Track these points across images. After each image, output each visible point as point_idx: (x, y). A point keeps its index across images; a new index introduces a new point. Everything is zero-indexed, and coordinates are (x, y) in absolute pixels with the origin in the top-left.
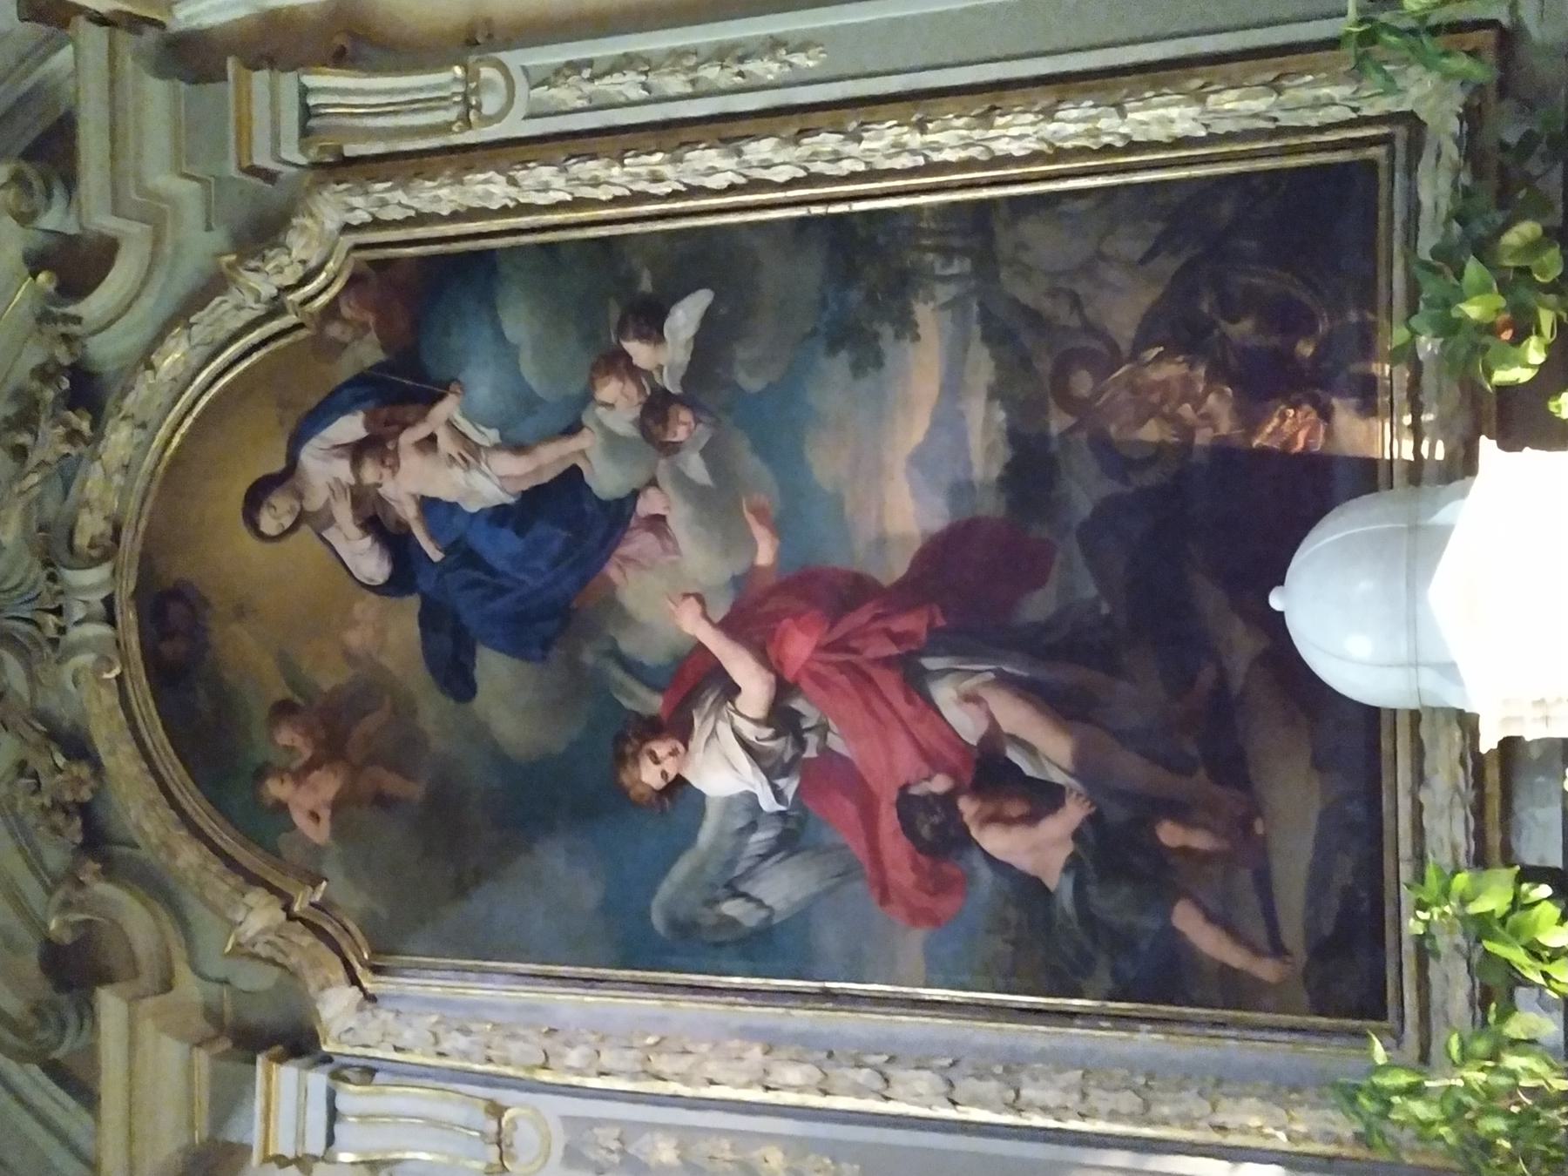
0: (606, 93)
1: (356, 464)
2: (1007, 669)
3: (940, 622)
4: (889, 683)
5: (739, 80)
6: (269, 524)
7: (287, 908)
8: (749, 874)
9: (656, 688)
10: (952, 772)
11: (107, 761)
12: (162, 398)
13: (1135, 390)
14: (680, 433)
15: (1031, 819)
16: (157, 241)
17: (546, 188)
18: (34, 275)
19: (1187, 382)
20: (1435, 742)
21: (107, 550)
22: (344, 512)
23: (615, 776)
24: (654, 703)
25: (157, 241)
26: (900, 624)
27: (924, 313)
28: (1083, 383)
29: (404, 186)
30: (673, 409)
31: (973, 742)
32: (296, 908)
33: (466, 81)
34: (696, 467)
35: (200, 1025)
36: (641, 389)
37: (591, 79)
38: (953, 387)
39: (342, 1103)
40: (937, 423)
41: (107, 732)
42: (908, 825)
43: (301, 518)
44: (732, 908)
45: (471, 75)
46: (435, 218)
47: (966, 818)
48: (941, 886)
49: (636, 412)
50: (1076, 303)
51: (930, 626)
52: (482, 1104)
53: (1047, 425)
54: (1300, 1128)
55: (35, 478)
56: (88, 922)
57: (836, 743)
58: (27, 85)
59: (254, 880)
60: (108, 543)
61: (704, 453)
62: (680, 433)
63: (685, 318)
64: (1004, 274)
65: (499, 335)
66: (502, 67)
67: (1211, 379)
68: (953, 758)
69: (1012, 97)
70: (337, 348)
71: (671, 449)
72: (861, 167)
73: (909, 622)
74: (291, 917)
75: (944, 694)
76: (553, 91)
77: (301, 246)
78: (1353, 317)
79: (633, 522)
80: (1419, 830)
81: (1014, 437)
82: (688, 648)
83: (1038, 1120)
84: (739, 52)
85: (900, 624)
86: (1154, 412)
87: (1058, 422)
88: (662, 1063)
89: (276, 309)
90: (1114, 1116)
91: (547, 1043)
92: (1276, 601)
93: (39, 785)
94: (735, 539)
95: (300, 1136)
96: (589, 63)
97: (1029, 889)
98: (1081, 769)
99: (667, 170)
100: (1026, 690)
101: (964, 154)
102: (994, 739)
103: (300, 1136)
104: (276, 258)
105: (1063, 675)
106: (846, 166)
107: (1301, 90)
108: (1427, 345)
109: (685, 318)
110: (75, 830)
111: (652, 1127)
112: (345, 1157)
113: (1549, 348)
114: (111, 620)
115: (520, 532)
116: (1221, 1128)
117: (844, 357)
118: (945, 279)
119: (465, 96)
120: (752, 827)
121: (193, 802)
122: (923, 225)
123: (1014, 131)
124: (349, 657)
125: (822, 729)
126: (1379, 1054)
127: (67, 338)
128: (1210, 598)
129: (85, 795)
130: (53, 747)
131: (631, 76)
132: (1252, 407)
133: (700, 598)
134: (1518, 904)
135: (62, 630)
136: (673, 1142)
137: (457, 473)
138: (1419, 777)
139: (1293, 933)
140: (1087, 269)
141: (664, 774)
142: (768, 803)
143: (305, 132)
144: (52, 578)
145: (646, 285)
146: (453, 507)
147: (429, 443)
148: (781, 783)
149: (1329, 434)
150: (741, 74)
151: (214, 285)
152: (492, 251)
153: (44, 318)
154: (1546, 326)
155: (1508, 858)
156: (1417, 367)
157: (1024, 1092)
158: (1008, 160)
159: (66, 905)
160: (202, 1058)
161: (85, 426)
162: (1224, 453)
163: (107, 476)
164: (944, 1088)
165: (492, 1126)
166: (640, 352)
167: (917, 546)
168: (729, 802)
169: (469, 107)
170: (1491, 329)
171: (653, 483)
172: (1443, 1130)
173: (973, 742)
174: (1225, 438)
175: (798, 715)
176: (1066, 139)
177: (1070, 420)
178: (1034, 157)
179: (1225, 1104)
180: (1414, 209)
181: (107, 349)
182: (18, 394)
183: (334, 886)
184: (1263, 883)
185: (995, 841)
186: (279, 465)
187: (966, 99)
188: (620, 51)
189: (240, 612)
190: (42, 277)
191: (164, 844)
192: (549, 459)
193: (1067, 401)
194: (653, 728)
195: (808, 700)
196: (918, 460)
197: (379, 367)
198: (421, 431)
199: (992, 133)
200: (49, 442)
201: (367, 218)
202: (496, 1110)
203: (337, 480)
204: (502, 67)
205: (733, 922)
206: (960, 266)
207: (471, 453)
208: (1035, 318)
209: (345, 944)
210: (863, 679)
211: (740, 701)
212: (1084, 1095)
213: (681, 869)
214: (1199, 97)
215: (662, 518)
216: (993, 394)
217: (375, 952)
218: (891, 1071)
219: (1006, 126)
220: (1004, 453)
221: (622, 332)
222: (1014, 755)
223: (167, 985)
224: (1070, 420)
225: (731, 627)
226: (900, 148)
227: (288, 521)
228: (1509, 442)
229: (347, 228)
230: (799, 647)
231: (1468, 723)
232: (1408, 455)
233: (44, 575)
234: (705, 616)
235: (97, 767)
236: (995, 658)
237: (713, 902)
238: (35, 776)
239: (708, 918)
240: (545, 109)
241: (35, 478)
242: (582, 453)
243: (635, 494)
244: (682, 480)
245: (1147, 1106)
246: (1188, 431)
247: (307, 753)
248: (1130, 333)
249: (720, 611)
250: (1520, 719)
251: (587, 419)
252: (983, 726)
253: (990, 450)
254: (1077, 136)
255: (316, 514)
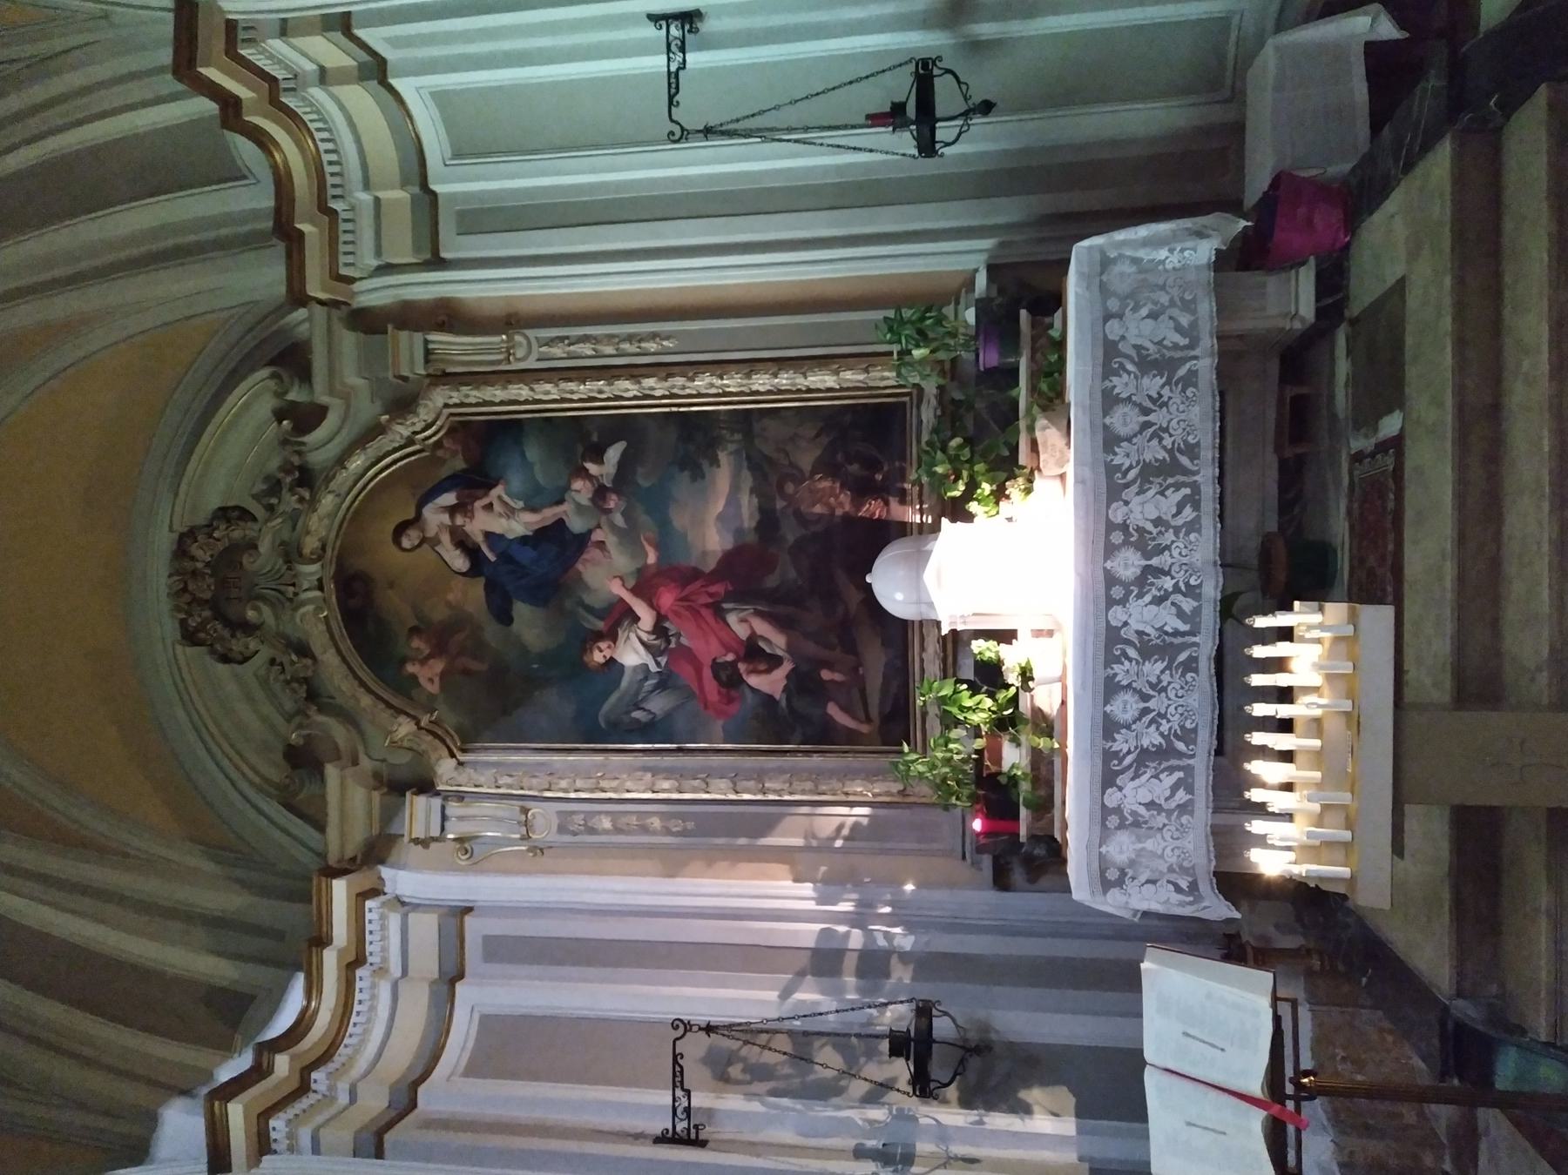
0: (575, 352)
1: (452, 517)
2: (760, 608)
3: (730, 588)
4: (706, 613)
5: (638, 350)
6: (406, 543)
7: (418, 724)
8: (644, 699)
9: (601, 618)
10: (736, 653)
11: (320, 657)
12: (349, 483)
13: (811, 491)
14: (612, 505)
15: (768, 671)
16: (348, 407)
17: (548, 393)
18: (280, 422)
19: (832, 488)
20: (928, 636)
21: (319, 555)
22: (446, 538)
23: (581, 658)
24: (600, 625)
25: (348, 407)
26: (713, 589)
27: (723, 457)
28: (790, 488)
29: (477, 388)
30: (608, 495)
31: (744, 639)
32: (422, 724)
33: (507, 342)
34: (619, 520)
35: (371, 781)
36: (593, 485)
37: (569, 345)
38: (735, 488)
39: (448, 812)
40: (728, 504)
41: (318, 640)
42: (716, 677)
43: (423, 540)
44: (637, 714)
45: (510, 339)
46: (493, 404)
47: (741, 671)
48: (730, 701)
49: (590, 496)
50: (787, 454)
51: (725, 589)
52: (518, 808)
53: (775, 505)
54: (876, 791)
55: (280, 520)
56: (309, 735)
57: (684, 641)
58: (275, 328)
59: (400, 712)
60: (320, 552)
61: (623, 514)
62: (612, 505)
63: (614, 454)
64: (757, 441)
65: (523, 455)
66: (527, 338)
67: (842, 486)
68: (734, 644)
69: (759, 366)
70: (442, 461)
71: (609, 511)
72: (695, 392)
73: (718, 588)
74: (420, 728)
75: (732, 619)
76: (551, 349)
77: (424, 414)
78: (897, 464)
79: (589, 544)
80: (923, 671)
81: (761, 510)
82: (615, 600)
83: (771, 797)
84: (639, 338)
85: (713, 589)
86: (819, 501)
87: (780, 504)
88: (603, 784)
89: (410, 442)
90: (803, 792)
91: (549, 778)
92: (868, 579)
93: (283, 668)
94: (638, 552)
95: (428, 828)
96: (567, 337)
97: (768, 700)
98: (790, 649)
99: (606, 389)
100: (758, 614)
101: (739, 389)
102: (753, 637)
103: (428, 828)
104: (412, 419)
105: (781, 609)
106: (688, 391)
107: (876, 373)
108: (925, 479)
109: (614, 454)
110: (302, 692)
111: (600, 813)
112: (451, 836)
113: (966, 484)
114: (321, 588)
115: (535, 548)
116: (847, 794)
117: (686, 473)
118: (732, 442)
119: (508, 349)
120: (646, 679)
121: (365, 674)
122: (722, 418)
123: (761, 382)
124: (449, 604)
125: (678, 635)
126: (906, 748)
127: (299, 453)
128: (842, 578)
129: (310, 673)
130: (290, 651)
131: (588, 345)
132: (858, 500)
133: (621, 578)
134: (956, 692)
135: (296, 594)
136: (609, 819)
137: (503, 521)
138: (923, 649)
139: (874, 712)
140: (793, 439)
141: (605, 657)
142: (653, 668)
143: (427, 361)
144: (289, 569)
145: (595, 438)
146: (501, 537)
147: (490, 507)
148: (659, 659)
149: (888, 511)
150: (639, 347)
151: (376, 430)
152: (520, 420)
153: (285, 442)
154: (965, 478)
155: (954, 675)
156: (921, 486)
157: (766, 785)
158: (757, 393)
159: (300, 726)
160: (376, 795)
161: (307, 495)
162: (848, 519)
163: (321, 519)
164: (731, 785)
165: (523, 818)
166: (593, 468)
167: (720, 555)
168: (635, 668)
169: (510, 354)
170: (946, 476)
171: (599, 526)
172: (928, 775)
173: (744, 639)
174: (847, 513)
175: (667, 629)
176: (783, 385)
177: (784, 504)
178: (769, 392)
179: (848, 783)
180: (920, 422)
181: (318, 458)
182: (267, 478)
183: (442, 712)
184: (863, 692)
185: (754, 681)
186: (411, 515)
187: (741, 365)
188: (582, 333)
189: (391, 585)
190: (285, 422)
191: (353, 696)
192: (549, 515)
193: (784, 496)
194: (599, 636)
195: (671, 623)
196: (720, 518)
197: (464, 471)
198: (485, 501)
199: (751, 381)
200: (290, 502)
201: (457, 401)
202: (525, 811)
203: (442, 523)
204: (527, 338)
205: (637, 721)
206: (738, 437)
207: (510, 512)
208: (769, 460)
209: (448, 741)
210: (696, 613)
211: (640, 624)
212: (791, 784)
213: (613, 699)
214: (836, 373)
215: (603, 542)
216: (752, 491)
217: (463, 742)
218: (708, 780)
219: (758, 379)
220: (757, 517)
221: (584, 460)
222: (762, 644)
223: (355, 762)
224: (784, 504)
225: (636, 591)
226: (712, 385)
227: (416, 543)
228: (953, 520)
229: (446, 406)
230: (667, 599)
231: (938, 624)
232: (918, 521)
233: (285, 567)
234: (623, 585)
235: (314, 658)
236: (754, 604)
237: (628, 713)
238: (281, 664)
239: (626, 719)
240: (547, 357)
241: (280, 520)
242: (565, 512)
243: (590, 532)
244: (614, 528)
245: (816, 786)
246: (832, 510)
247: (427, 651)
248: (809, 468)
249: (631, 583)
250: (955, 623)
251: (567, 497)
252: (749, 632)
253: (751, 515)
254: (786, 385)
255: (430, 539)
